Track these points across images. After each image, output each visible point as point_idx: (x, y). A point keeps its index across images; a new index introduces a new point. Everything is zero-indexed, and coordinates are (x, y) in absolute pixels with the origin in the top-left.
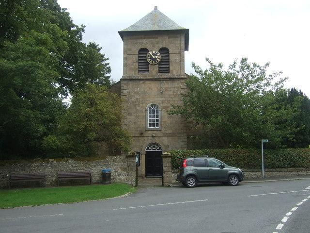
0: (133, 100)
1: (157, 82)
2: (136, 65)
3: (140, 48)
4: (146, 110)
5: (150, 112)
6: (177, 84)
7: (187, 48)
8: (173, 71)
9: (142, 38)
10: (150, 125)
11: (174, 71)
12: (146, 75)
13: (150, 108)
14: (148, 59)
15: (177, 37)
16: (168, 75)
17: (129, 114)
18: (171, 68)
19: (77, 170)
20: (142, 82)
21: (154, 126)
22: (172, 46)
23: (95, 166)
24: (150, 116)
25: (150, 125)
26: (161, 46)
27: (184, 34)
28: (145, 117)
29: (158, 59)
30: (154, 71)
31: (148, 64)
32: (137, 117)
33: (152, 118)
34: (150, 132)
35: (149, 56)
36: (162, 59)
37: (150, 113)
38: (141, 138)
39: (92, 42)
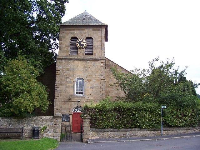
0: (65, 74)
1: (81, 61)
2: (69, 49)
3: (72, 36)
4: (74, 82)
5: (77, 84)
6: (98, 63)
7: (106, 40)
8: (80, 54)
9: (74, 30)
10: (77, 93)
11: (97, 53)
12: (75, 56)
13: (77, 81)
14: (77, 44)
15: (100, 30)
16: (93, 57)
17: (61, 84)
18: (94, 52)
19: (12, 126)
20: (72, 61)
21: (80, 93)
22: (97, 35)
23: (27, 124)
24: (77, 86)
25: (77, 93)
26: (87, 36)
27: (106, 27)
28: (73, 87)
29: (84, 45)
30: (82, 53)
31: (77, 48)
32: (67, 87)
33: (81, 85)
34: (76, 98)
35: (78, 42)
36: (88, 45)
37: (31, 110)
38: (69, 103)
39: (179, 66)
